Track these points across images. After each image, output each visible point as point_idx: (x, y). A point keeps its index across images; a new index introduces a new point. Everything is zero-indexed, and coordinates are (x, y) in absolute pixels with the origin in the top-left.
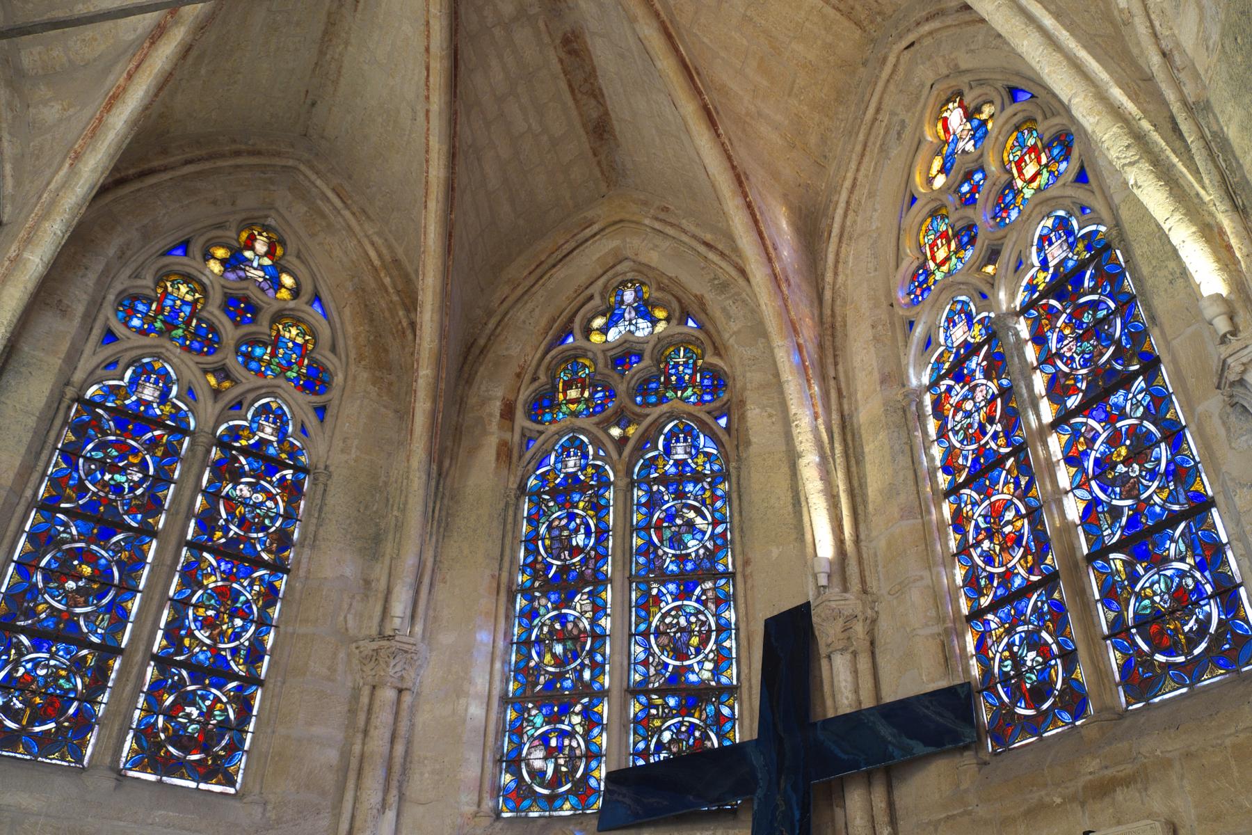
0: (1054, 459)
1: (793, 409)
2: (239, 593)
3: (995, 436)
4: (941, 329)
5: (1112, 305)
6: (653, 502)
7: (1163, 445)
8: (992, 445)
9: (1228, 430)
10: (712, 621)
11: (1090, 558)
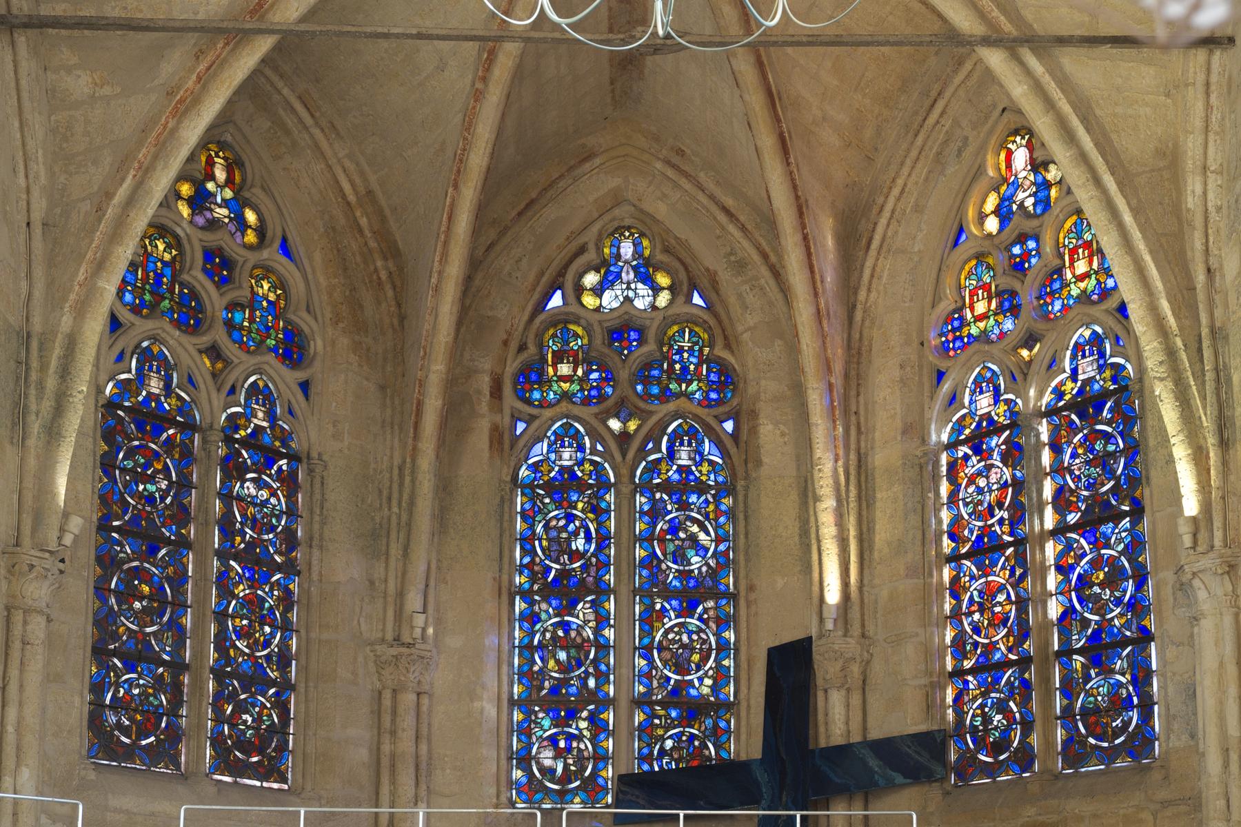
0: (1048, 564)
1: (818, 453)
2: (263, 600)
3: (1001, 522)
4: (968, 390)
5: (1121, 445)
6: (655, 513)
7: (1131, 581)
8: (997, 528)
9: (1175, 599)
10: (713, 639)
11: (1058, 654)
